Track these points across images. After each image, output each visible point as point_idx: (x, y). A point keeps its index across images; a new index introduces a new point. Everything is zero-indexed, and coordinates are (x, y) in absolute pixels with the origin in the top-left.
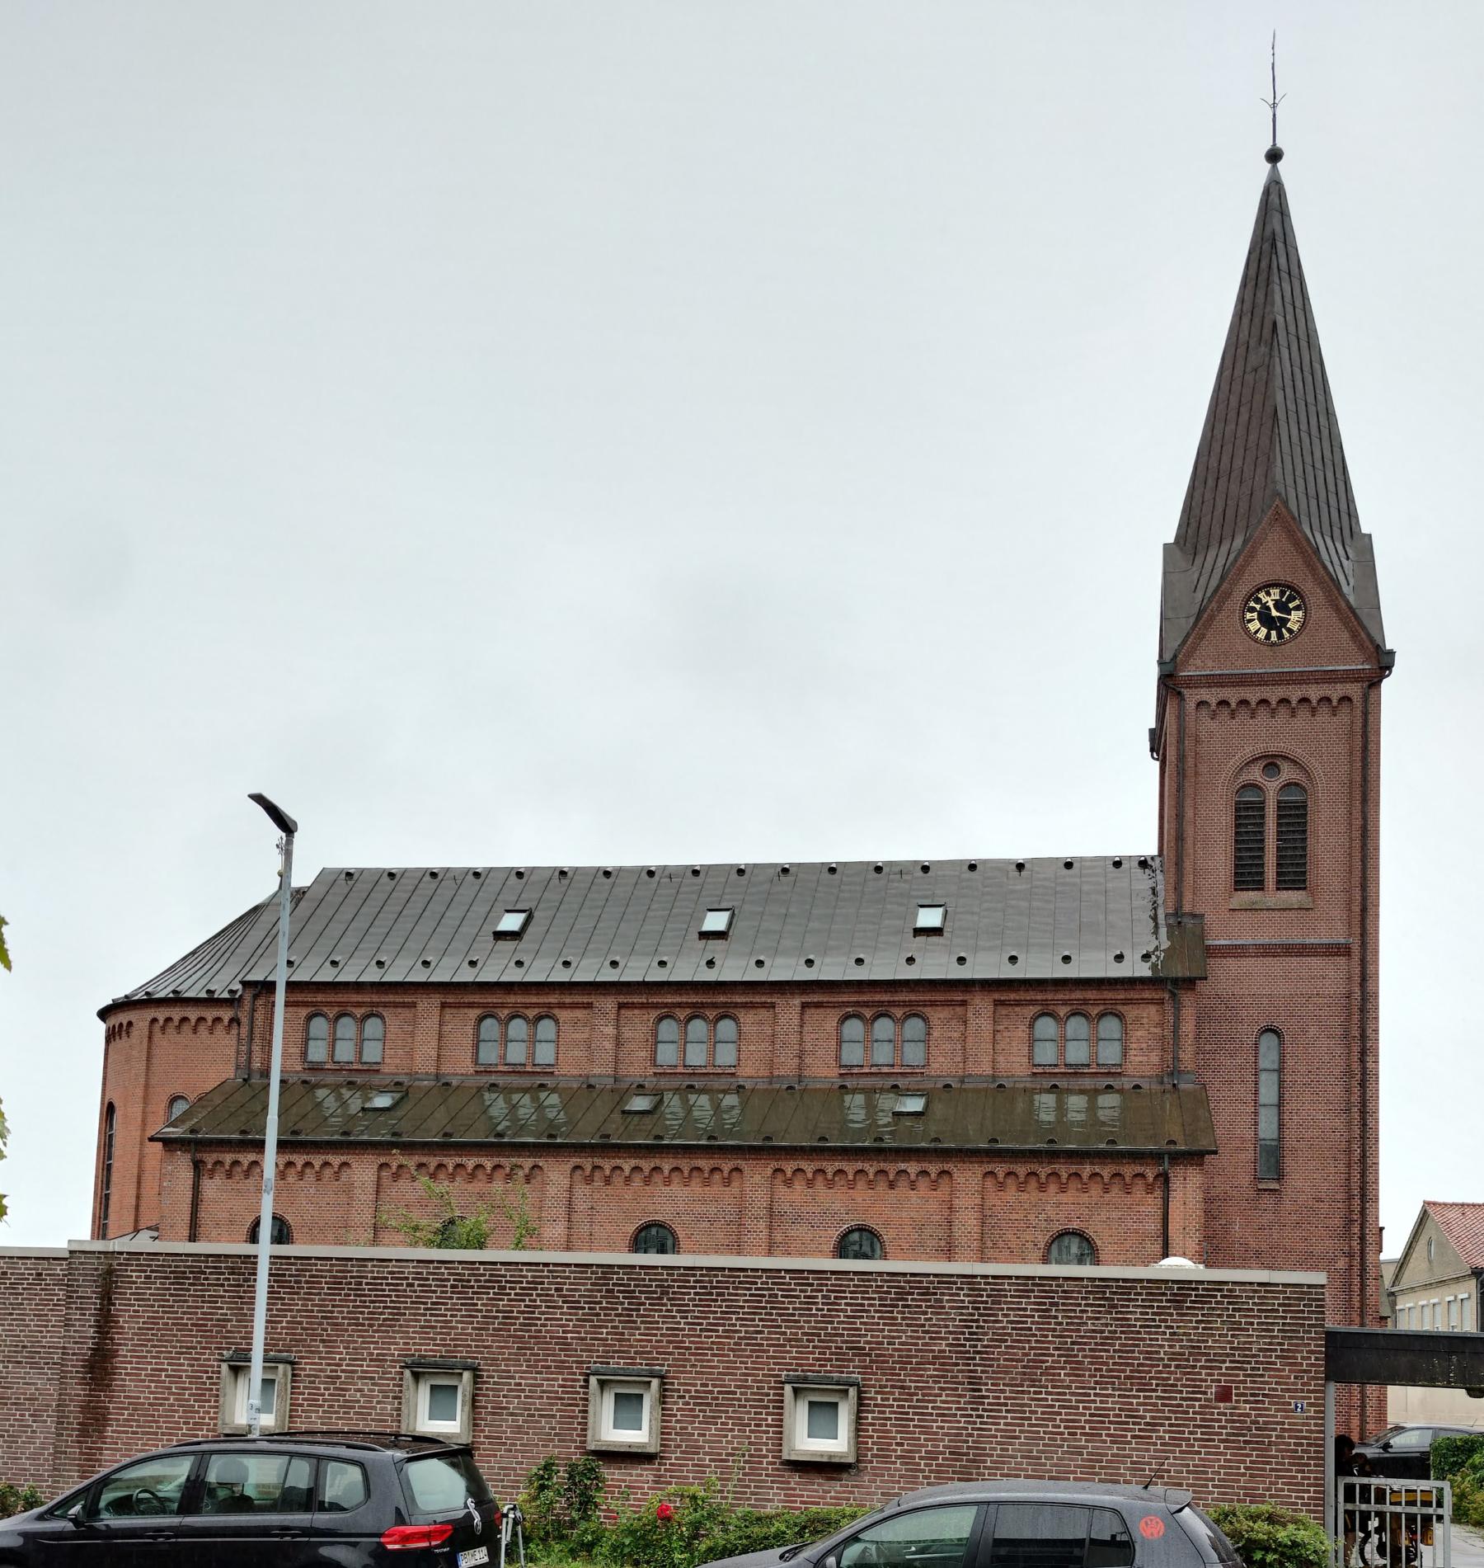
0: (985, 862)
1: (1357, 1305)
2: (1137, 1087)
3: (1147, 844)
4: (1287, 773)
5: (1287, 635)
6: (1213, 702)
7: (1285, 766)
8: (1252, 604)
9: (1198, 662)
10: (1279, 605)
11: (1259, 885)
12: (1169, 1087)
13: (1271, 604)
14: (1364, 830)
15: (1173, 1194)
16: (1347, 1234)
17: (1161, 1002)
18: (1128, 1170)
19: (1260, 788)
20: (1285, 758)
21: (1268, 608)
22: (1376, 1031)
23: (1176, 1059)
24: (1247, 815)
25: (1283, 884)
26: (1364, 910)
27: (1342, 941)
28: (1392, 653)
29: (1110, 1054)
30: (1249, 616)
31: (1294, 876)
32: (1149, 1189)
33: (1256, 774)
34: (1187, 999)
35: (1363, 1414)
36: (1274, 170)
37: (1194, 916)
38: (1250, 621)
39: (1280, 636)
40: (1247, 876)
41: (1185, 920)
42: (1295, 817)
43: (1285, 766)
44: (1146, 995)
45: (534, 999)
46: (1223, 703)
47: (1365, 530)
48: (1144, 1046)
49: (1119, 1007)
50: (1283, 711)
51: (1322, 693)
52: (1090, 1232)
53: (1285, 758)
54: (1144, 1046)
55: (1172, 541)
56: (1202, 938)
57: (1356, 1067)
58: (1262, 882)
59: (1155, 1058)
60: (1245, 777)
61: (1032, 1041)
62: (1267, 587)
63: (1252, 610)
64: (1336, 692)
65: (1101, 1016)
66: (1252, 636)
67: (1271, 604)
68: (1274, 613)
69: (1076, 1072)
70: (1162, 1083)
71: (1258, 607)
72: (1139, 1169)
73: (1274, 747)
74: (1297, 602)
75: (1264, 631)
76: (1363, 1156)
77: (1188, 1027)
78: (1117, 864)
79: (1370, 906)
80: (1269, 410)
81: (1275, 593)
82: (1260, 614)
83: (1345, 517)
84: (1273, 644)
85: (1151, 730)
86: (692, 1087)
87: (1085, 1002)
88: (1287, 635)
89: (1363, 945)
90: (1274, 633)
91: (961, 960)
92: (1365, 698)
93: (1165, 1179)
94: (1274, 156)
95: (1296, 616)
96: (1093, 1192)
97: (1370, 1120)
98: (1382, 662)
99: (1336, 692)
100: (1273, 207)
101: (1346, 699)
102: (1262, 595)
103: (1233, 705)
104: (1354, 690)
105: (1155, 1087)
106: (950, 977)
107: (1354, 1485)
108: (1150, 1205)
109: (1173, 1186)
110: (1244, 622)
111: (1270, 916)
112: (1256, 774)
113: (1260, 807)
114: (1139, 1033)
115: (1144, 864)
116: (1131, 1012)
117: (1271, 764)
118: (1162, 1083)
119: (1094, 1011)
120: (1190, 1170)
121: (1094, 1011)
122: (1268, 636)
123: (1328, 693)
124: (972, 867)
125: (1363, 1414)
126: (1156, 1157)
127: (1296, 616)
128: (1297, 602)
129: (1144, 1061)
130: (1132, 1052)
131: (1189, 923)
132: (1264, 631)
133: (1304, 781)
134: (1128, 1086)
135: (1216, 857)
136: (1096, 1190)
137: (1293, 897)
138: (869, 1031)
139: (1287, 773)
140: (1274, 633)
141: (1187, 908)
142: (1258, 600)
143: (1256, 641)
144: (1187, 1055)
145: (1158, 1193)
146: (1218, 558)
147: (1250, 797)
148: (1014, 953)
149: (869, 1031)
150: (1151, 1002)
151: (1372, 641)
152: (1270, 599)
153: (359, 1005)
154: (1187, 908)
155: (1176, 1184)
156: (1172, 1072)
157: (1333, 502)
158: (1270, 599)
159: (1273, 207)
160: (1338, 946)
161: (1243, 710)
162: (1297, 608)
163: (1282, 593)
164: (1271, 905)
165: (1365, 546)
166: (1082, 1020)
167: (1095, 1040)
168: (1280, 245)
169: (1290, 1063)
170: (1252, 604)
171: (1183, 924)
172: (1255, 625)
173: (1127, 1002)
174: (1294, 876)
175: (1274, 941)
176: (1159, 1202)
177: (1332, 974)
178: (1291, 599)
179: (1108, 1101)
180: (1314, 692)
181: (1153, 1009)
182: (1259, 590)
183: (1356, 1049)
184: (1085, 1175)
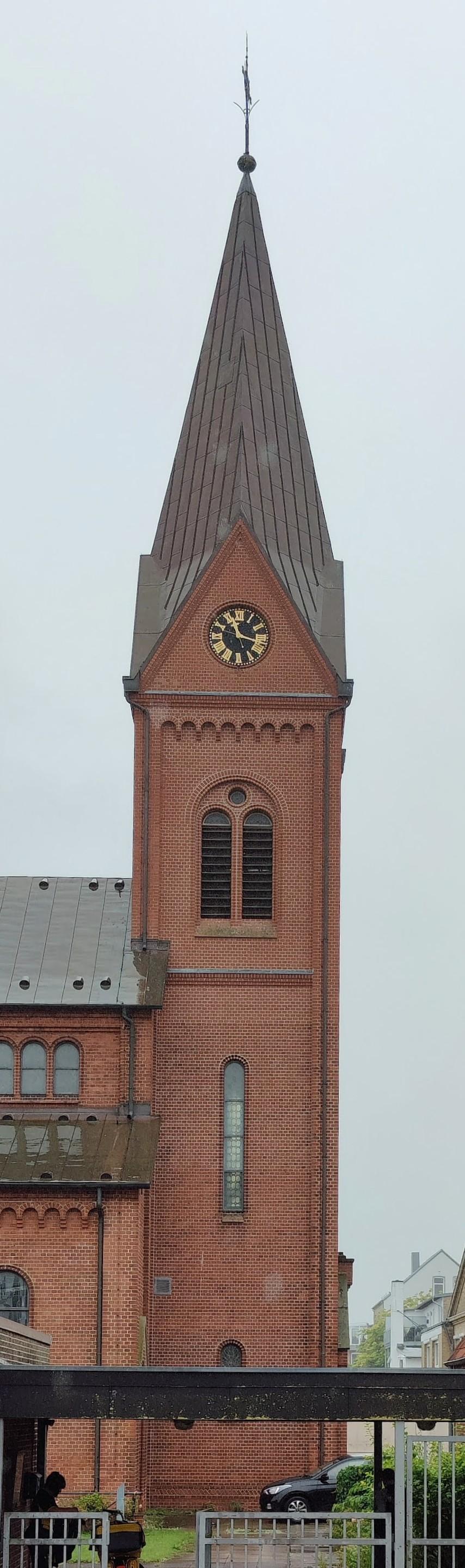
0: (58, 879)
1: (317, 1337)
2: (91, 1118)
3: (121, 866)
4: (253, 800)
5: (251, 658)
6: (258, 725)
7: (250, 792)
8: (217, 624)
9: (163, 680)
10: (244, 627)
11: (225, 913)
12: (123, 1118)
13: (235, 625)
14: (325, 860)
15: (107, 1230)
16: (308, 1267)
17: (117, 1031)
18: (63, 1204)
19: (227, 815)
20: (250, 784)
21: (233, 629)
22: (336, 1062)
23: (132, 1089)
24: (214, 842)
25: (247, 913)
26: (325, 940)
27: (305, 971)
28: (351, 682)
29: (67, 1084)
30: (214, 636)
31: (259, 902)
32: (85, 1225)
33: (221, 799)
34: (144, 1030)
35: (321, 1447)
36: (247, 182)
37: (160, 943)
38: (216, 641)
39: (245, 659)
40: (213, 902)
41: (152, 946)
42: (260, 845)
43: (250, 792)
44: (103, 1023)
45: (24, 1023)
46: (188, 724)
47: (337, 557)
48: (101, 1076)
49: (77, 1036)
50: (267, 735)
51: (224, 719)
52: (25, 1270)
53: (250, 784)
54: (101, 1076)
55: (148, 551)
56: (167, 967)
57: (317, 1098)
58: (229, 910)
59: (111, 1088)
60: (207, 805)
61: (19, 1069)
62: (231, 608)
63: (217, 630)
64: (297, 719)
65: (58, 1044)
66: (217, 657)
67: (235, 625)
68: (239, 635)
69: (31, 1102)
70: (118, 1114)
71: (223, 627)
72: (74, 1204)
73: (244, 771)
74: (261, 625)
75: (229, 653)
76: (324, 1188)
77: (144, 1058)
78: (94, 886)
79: (331, 938)
80: (236, 427)
81: (240, 615)
82: (225, 634)
83: (316, 542)
84: (239, 667)
85: (125, 679)
86: (65, 1118)
87: (41, 1029)
88: (251, 658)
89: (324, 978)
90: (238, 655)
91: (25, 984)
92: (326, 726)
93: (99, 1212)
94: (247, 164)
95: (260, 639)
96: (28, 1228)
97: (329, 1153)
98: (341, 694)
99: (297, 719)
100: (246, 210)
101: (306, 726)
102: (227, 616)
103: (199, 727)
104: (315, 718)
105: (111, 1118)
106: (10, 1002)
107: (69, 1536)
108: (85, 1242)
109: (107, 1221)
110: (210, 642)
111: (233, 944)
112: (221, 799)
113: (227, 833)
114: (96, 1063)
115: (120, 886)
116: (88, 1040)
117: (237, 788)
118: (118, 1114)
119: (51, 1039)
120: (125, 1203)
121: (51, 1039)
122: (233, 659)
123: (291, 720)
124: (44, 885)
125: (321, 1447)
126: (88, 1191)
127: (260, 639)
128: (261, 625)
129: (101, 1094)
130: (90, 1082)
131: (154, 949)
132: (229, 653)
133: (268, 807)
134: (83, 1117)
135: (185, 885)
136: (30, 1226)
137: (257, 926)
138: (51, 1058)
139: (253, 800)
140: (238, 655)
141: (153, 935)
142: (223, 621)
143: (222, 662)
144: (144, 1088)
145: (93, 1228)
146: (186, 575)
147: (217, 823)
148: (26, 978)
149: (51, 1058)
150: (108, 1030)
151: (331, 667)
152: (235, 620)
153: (20, 1030)
154: (153, 935)
155: (111, 1219)
156: (128, 1103)
157: (303, 526)
158: (235, 620)
159: (246, 210)
160: (300, 977)
161: (267, 734)
162: (261, 631)
163: (247, 616)
164: (236, 933)
165: (331, 573)
166: (39, 1048)
167: (52, 1070)
168: (251, 260)
169: (254, 1095)
170: (217, 624)
171: (149, 953)
172: (219, 647)
173: (83, 1030)
174: (259, 902)
175: (239, 970)
176: (95, 1237)
177: (291, 1005)
178: (255, 621)
179: (65, 1132)
180: (239, 718)
181: (109, 1038)
182: (225, 610)
183: (317, 1081)
184: (19, 1211)
